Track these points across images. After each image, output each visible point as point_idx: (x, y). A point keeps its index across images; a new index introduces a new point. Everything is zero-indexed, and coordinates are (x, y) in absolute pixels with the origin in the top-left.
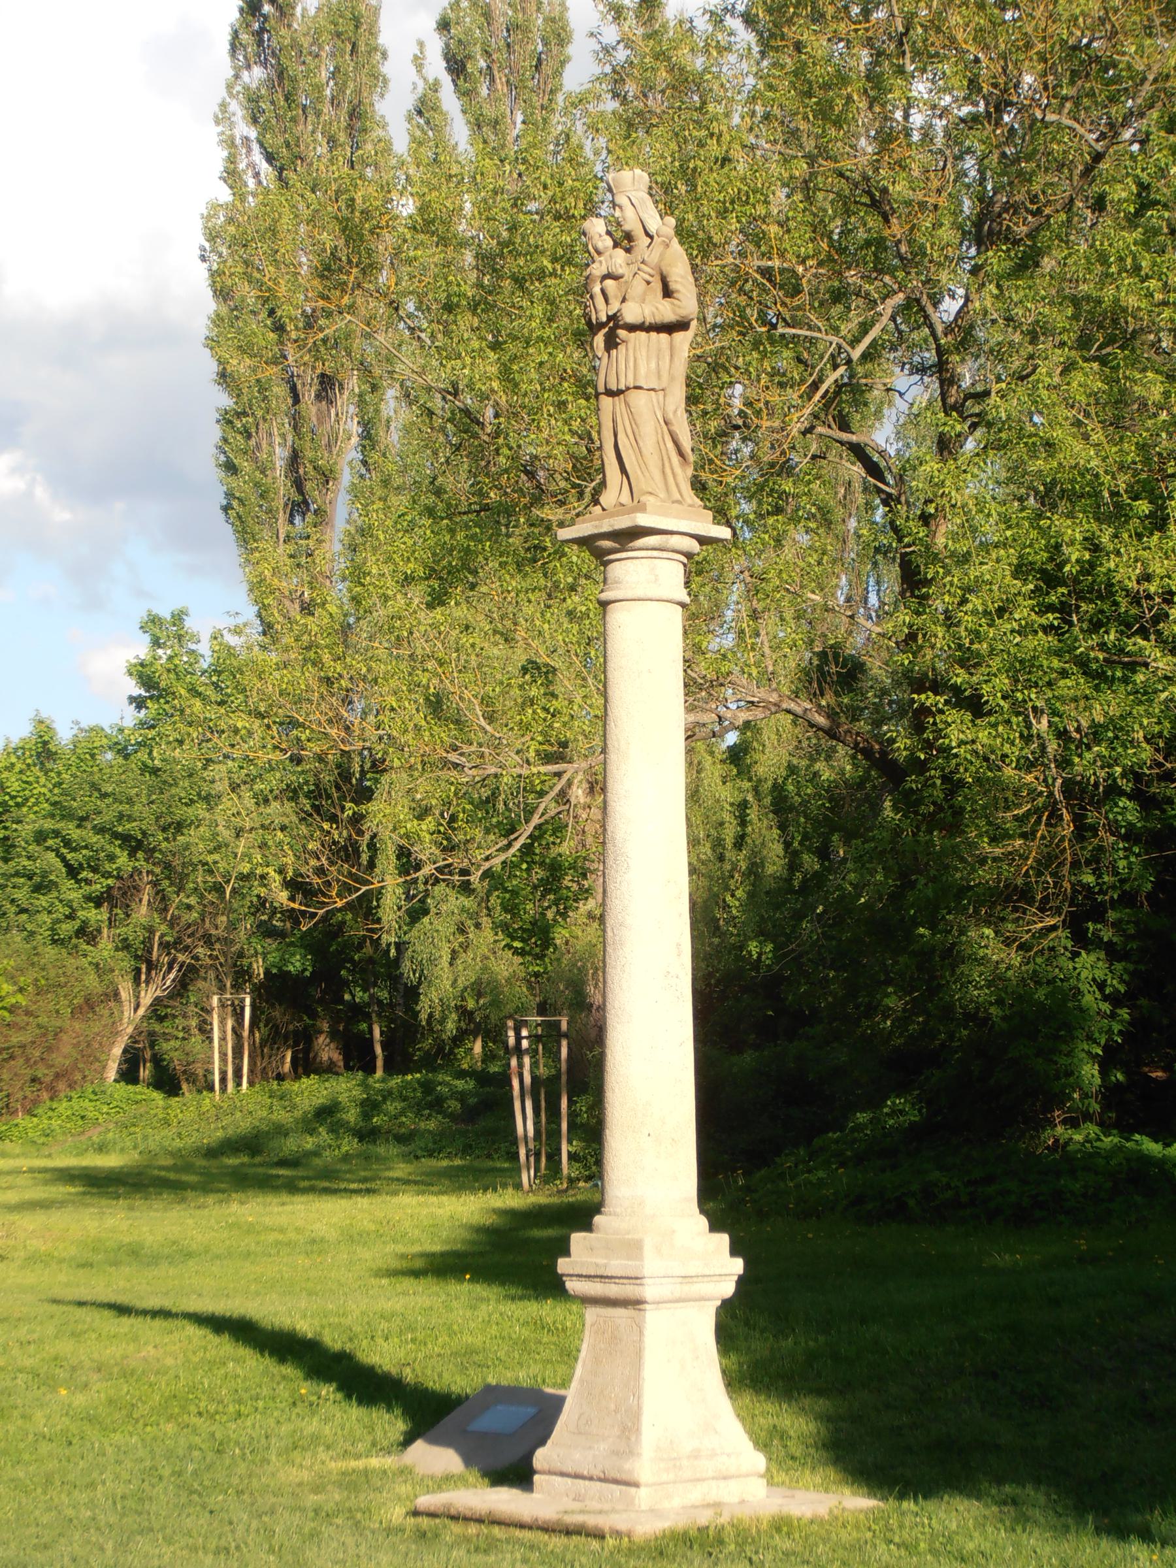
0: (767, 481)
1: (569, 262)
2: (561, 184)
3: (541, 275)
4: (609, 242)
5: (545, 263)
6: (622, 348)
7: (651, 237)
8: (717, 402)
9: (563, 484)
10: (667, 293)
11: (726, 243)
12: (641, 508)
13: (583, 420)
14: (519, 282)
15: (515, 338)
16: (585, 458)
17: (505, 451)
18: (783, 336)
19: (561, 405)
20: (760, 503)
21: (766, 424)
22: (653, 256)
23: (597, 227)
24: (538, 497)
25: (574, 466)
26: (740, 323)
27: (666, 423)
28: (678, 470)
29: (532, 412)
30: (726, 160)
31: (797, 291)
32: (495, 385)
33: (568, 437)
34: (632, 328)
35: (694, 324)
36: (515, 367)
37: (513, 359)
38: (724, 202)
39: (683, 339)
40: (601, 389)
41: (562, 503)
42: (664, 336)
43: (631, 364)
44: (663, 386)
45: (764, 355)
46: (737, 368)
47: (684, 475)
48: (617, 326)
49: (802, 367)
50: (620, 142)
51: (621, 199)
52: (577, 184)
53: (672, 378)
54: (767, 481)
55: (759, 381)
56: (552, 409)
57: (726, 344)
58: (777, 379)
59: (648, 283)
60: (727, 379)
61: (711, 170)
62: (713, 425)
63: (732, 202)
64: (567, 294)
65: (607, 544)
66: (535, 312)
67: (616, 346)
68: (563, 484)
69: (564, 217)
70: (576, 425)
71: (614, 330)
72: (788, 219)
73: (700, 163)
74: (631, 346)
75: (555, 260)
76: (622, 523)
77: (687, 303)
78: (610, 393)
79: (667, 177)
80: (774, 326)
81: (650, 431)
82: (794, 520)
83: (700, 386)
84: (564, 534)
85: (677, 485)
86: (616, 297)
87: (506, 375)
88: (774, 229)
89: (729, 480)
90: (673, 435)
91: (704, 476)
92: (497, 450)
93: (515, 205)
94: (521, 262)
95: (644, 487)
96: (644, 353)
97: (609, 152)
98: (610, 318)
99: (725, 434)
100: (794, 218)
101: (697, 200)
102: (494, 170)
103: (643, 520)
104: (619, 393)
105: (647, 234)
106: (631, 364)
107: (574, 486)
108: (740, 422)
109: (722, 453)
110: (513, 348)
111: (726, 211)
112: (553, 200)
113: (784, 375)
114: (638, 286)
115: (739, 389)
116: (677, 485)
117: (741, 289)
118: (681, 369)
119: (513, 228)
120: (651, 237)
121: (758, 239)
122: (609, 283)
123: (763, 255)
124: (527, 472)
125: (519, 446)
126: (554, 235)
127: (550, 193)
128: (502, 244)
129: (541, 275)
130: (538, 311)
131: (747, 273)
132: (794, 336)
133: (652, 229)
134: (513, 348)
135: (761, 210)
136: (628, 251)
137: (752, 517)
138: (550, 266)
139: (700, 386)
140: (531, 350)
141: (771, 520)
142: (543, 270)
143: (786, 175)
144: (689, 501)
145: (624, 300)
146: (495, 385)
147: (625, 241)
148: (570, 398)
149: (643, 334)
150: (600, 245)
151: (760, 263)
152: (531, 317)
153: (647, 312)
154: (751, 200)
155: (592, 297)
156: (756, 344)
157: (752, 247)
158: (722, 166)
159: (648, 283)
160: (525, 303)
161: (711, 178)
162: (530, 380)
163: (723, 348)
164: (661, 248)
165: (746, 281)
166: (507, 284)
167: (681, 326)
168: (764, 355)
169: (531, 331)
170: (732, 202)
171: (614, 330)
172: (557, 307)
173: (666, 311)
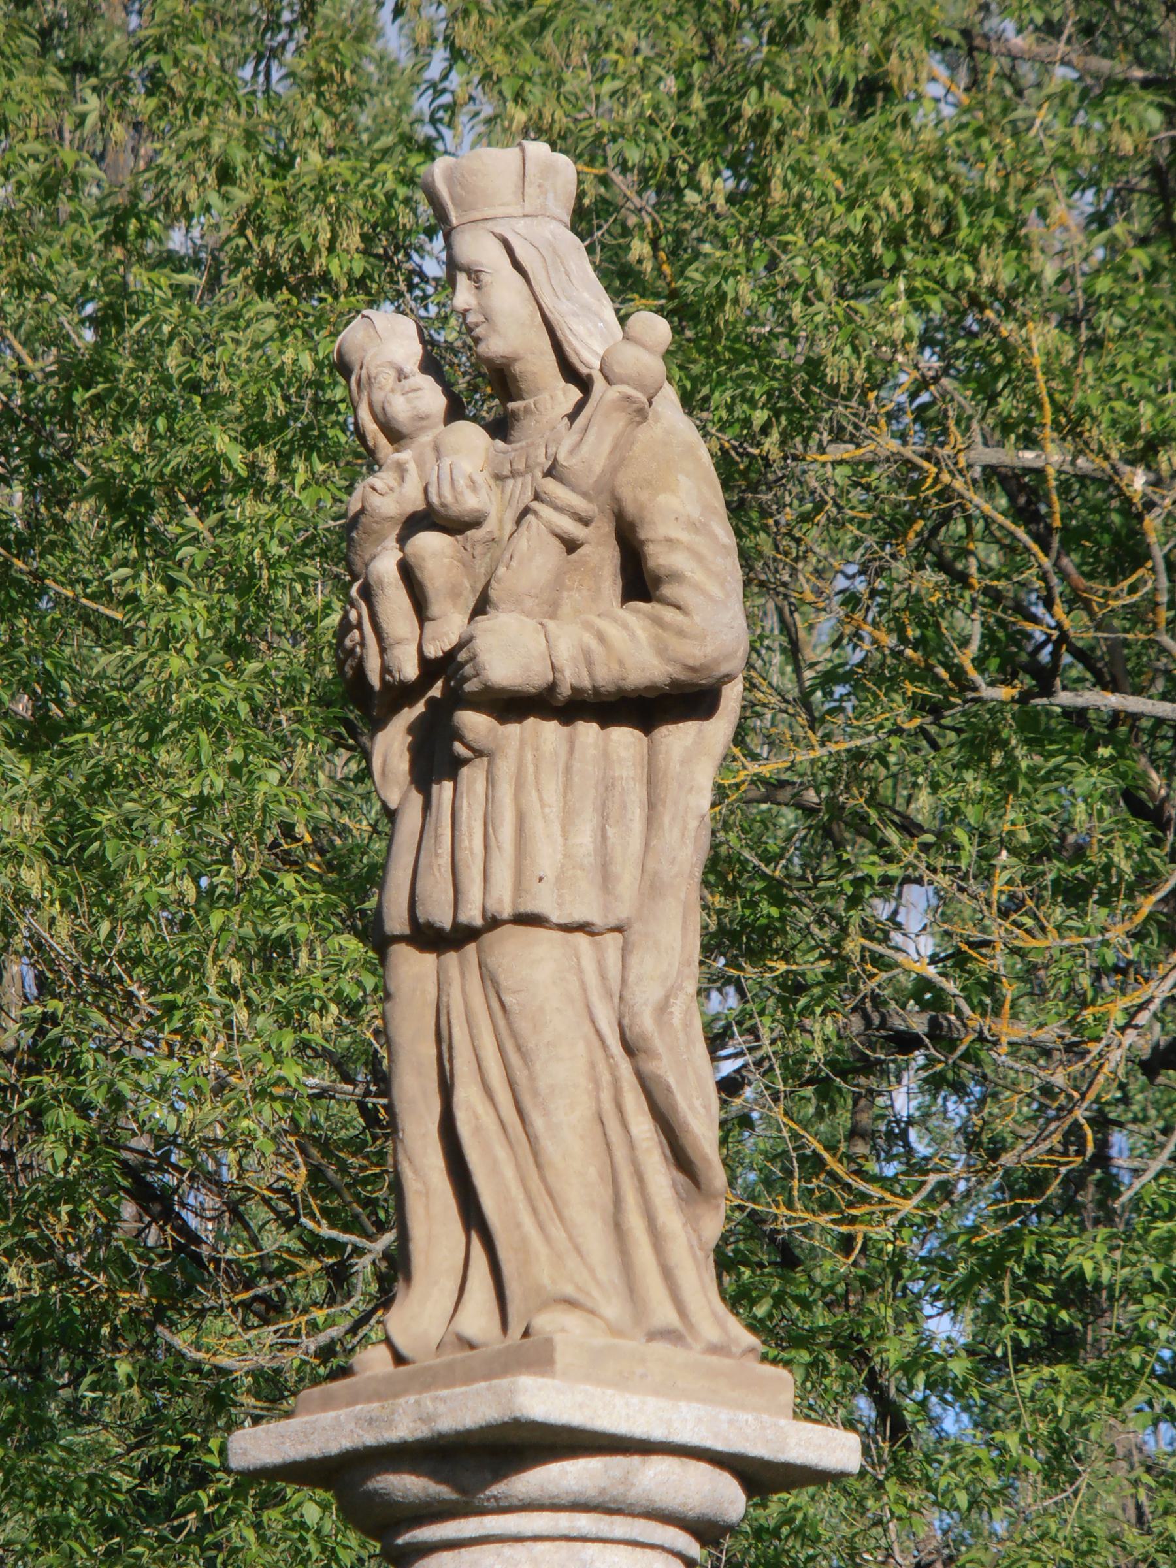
0: (1013, 1237)
1: (311, 443)
2: (282, 165)
3: (208, 486)
4: (433, 398)
5: (223, 443)
6: (473, 776)
7: (584, 383)
8: (834, 953)
9: (275, 1239)
10: (639, 581)
11: (876, 384)
12: (534, 1354)
13: (352, 1009)
14: (127, 505)
15: (111, 711)
16: (356, 1146)
17: (64, 1117)
18: (1077, 717)
19: (274, 955)
20: (991, 1315)
21: (1010, 1031)
22: (590, 450)
23: (387, 340)
24: (185, 1276)
25: (316, 1173)
26: (918, 666)
27: (630, 1050)
28: (671, 1219)
29: (171, 978)
30: (873, 91)
31: (1128, 553)
32: (33, 878)
33: (292, 1071)
34: (512, 706)
35: (732, 696)
36: (106, 817)
37: (102, 784)
38: (866, 240)
39: (695, 752)
40: (396, 921)
41: (270, 1309)
42: (624, 737)
43: (506, 832)
44: (622, 911)
45: (1007, 783)
46: (909, 827)
47: (690, 1236)
48: (457, 699)
49: (1142, 831)
50: (496, 23)
51: (478, 247)
52: (338, 165)
53: (652, 888)
54: (1013, 1237)
55: (986, 875)
56: (236, 969)
57: (870, 742)
58: (1052, 870)
59: (571, 546)
60: (871, 866)
61: (820, 124)
62: (821, 1034)
63: (896, 240)
64: (297, 555)
65: (407, 1485)
66: (182, 619)
67: (452, 767)
68: (275, 1239)
69: (291, 280)
70: (323, 1024)
71: (446, 711)
72: (1093, 303)
73: (779, 102)
74: (505, 768)
75: (255, 434)
76: (466, 1409)
77: (711, 616)
78: (430, 938)
79: (665, 148)
80: (1045, 679)
81: (570, 1076)
82: (1112, 1381)
83: (775, 892)
84: (256, 1445)
85: (667, 1274)
86: (455, 594)
87: (72, 843)
88: (1042, 339)
89: (881, 1232)
90: (649, 1089)
91: (784, 1217)
92: (37, 1112)
93: (116, 236)
94: (136, 436)
95: (545, 1274)
96: (552, 789)
97: (457, 55)
98: (431, 668)
99: (868, 1067)
100: (1114, 301)
101: (769, 230)
102: (45, 112)
103: (542, 1400)
104: (459, 937)
105: (570, 372)
106: (506, 832)
107: (315, 1246)
108: (919, 1024)
109: (855, 1133)
110: (99, 746)
111: (872, 270)
112: (251, 220)
113: (1079, 854)
114: (533, 559)
115: (916, 905)
116: (667, 1274)
117: (925, 543)
118: (684, 849)
119: (108, 321)
120: (584, 383)
121: (992, 371)
122: (429, 542)
123: (1006, 426)
124: (144, 1194)
125: (117, 1101)
126: (256, 342)
127: (242, 196)
128: (79, 372)
129: (208, 486)
130: (193, 613)
131: (945, 494)
132: (1116, 717)
133: (588, 356)
134: (99, 746)
135: (997, 270)
136: (500, 428)
137: (959, 1367)
138: (237, 456)
139: (775, 892)
140: (166, 756)
141: (1028, 1380)
142: (213, 465)
143: (1087, 148)
144: (710, 1333)
145: (482, 606)
146: (33, 878)
147: (485, 391)
148: (304, 931)
149: (550, 731)
150: (400, 409)
151: (993, 456)
152: (168, 638)
153: (565, 652)
154: (964, 235)
155: (367, 593)
156: (979, 744)
157: (963, 397)
158: (862, 111)
159: (571, 546)
160: (148, 588)
161: (818, 154)
162: (156, 869)
163: (858, 755)
164: (618, 423)
165: (946, 517)
166: (83, 512)
167: (689, 699)
168: (1007, 783)
169: (169, 687)
170: (896, 240)
171: (446, 711)
172: (264, 603)
173: (635, 649)
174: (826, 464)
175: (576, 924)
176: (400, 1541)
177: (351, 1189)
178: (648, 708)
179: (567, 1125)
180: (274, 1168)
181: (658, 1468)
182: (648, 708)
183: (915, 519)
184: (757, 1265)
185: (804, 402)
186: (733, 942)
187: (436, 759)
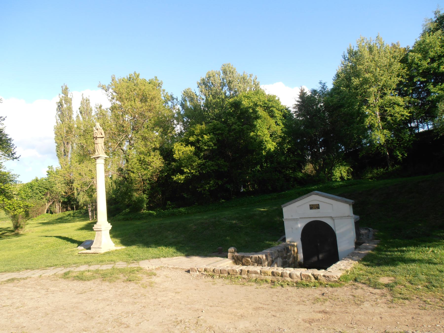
23: (94, 128)
24: (90, 154)
39: (103, 139)
47: (104, 152)
71: (96, 138)
77: (104, 135)
81: (100, 147)
114: (99, 134)
118: (103, 142)
121: (111, 130)
147: (97, 130)
171: (96, 138)
173: (102, 136)
174: (107, 132)
175: (100, 143)
176: (425, 80)
177: (94, 151)
178: (102, 138)
179: (100, 149)
180: (92, 151)
181: (34, 226)
182: (102, 138)
183: (109, 133)
184: (106, 153)
185: (106, 130)
186: (105, 144)
187: (96, 139)
